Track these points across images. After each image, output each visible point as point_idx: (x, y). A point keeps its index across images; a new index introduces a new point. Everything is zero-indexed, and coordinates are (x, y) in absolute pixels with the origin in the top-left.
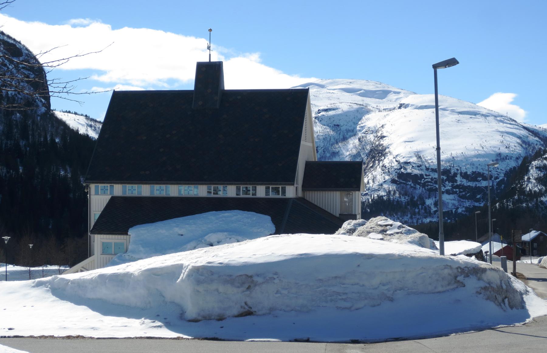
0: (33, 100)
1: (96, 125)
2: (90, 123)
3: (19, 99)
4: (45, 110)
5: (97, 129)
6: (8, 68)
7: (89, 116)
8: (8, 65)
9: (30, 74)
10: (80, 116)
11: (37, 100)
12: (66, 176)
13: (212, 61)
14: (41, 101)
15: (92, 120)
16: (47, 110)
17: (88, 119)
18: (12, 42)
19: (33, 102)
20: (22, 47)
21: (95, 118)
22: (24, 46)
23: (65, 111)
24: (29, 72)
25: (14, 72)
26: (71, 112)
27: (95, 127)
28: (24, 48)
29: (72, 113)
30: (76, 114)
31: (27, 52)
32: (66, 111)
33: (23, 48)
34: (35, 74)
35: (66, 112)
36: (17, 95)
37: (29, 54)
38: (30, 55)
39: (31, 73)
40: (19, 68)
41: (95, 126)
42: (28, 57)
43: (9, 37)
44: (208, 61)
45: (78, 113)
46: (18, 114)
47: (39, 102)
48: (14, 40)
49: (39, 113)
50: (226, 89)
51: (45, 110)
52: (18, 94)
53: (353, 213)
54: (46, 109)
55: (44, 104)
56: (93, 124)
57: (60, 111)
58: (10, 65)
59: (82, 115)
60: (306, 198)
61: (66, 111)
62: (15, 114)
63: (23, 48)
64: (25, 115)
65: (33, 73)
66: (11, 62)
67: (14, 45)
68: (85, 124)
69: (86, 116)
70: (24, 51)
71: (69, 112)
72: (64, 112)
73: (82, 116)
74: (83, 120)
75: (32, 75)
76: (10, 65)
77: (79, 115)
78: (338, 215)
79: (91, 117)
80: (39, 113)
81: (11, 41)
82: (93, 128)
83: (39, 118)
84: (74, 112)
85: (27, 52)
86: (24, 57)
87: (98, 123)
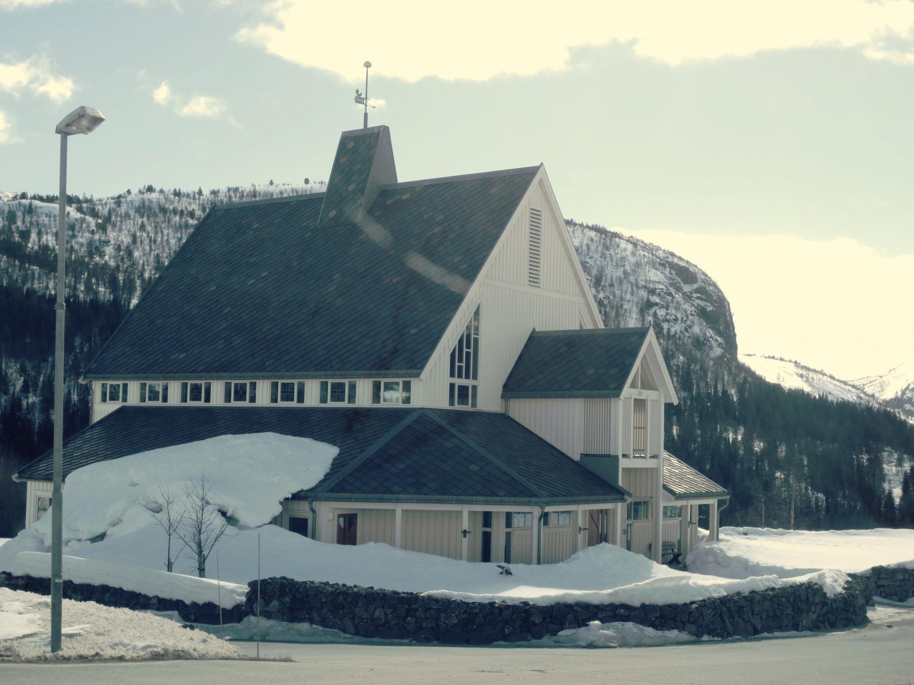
0: (705, 339)
1: (809, 375)
2: (800, 372)
3: (686, 338)
4: (721, 352)
5: (810, 379)
6: (673, 297)
7: (800, 363)
8: (674, 293)
9: (707, 306)
10: (788, 363)
11: (711, 339)
12: (735, 440)
13: (369, 126)
14: (716, 340)
15: (804, 368)
16: (724, 352)
17: (798, 366)
18: (684, 264)
19: (705, 342)
20: (697, 270)
21: (807, 365)
22: (699, 270)
23: (768, 356)
24: (706, 303)
25: (681, 302)
26: (776, 357)
27: (807, 378)
28: (700, 272)
29: (777, 359)
30: (782, 359)
31: (703, 277)
32: (769, 356)
33: (699, 271)
34: (713, 306)
35: (769, 357)
36: (683, 332)
37: (706, 280)
38: (707, 281)
39: (709, 304)
40: (693, 298)
41: (807, 376)
42: (705, 283)
43: (680, 259)
44: (362, 127)
45: (785, 358)
46: (681, 357)
47: (713, 342)
48: (687, 262)
49: (712, 355)
50: (399, 182)
51: (721, 352)
52: (684, 332)
53: (612, 453)
54: (723, 351)
55: (721, 344)
56: (804, 372)
57: (761, 357)
58: (676, 293)
59: (790, 361)
60: (511, 415)
61: (769, 356)
62: (677, 357)
63: (699, 271)
64: (691, 359)
65: (712, 304)
66: (678, 289)
67: (687, 269)
68: (794, 373)
69: (796, 362)
70: (700, 276)
71: (773, 358)
72: (766, 357)
73: (790, 363)
74: (792, 368)
75: (709, 306)
76: (676, 293)
77: (786, 361)
78: (576, 457)
79: (802, 364)
80: (712, 355)
81: (682, 264)
82: (804, 379)
83: (711, 363)
84: (779, 358)
85: (703, 277)
86: (699, 283)
87: (811, 372)
